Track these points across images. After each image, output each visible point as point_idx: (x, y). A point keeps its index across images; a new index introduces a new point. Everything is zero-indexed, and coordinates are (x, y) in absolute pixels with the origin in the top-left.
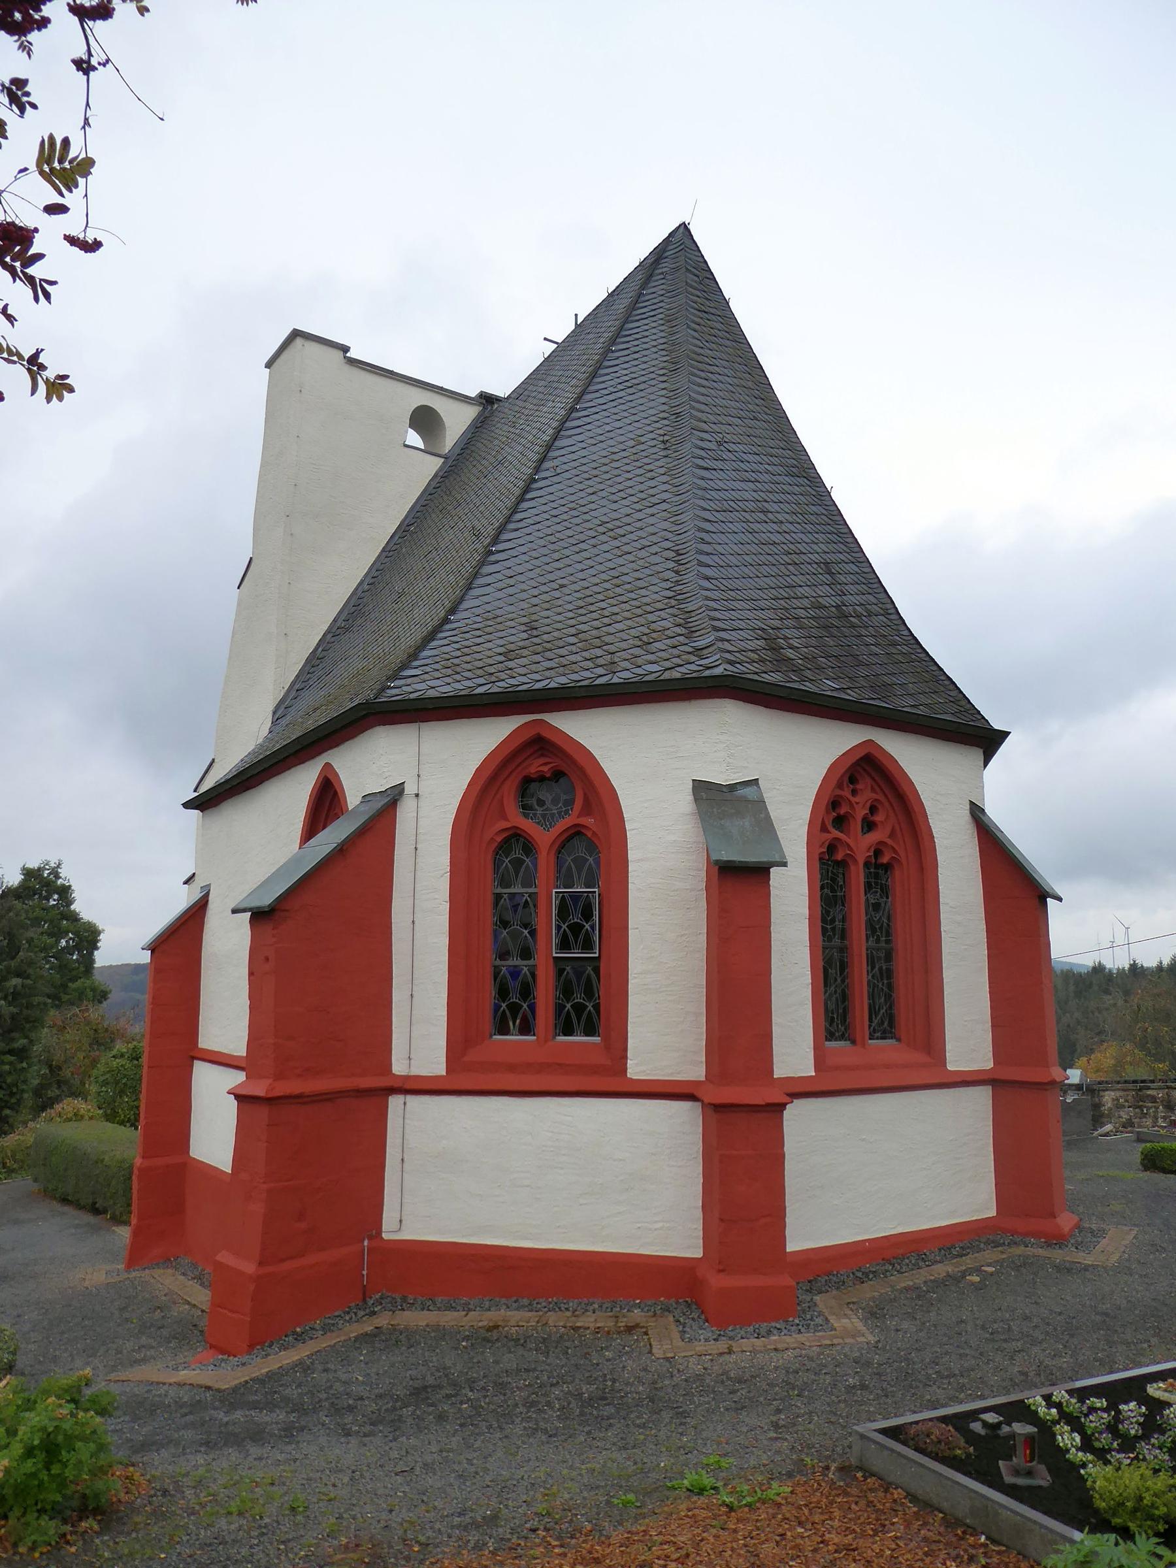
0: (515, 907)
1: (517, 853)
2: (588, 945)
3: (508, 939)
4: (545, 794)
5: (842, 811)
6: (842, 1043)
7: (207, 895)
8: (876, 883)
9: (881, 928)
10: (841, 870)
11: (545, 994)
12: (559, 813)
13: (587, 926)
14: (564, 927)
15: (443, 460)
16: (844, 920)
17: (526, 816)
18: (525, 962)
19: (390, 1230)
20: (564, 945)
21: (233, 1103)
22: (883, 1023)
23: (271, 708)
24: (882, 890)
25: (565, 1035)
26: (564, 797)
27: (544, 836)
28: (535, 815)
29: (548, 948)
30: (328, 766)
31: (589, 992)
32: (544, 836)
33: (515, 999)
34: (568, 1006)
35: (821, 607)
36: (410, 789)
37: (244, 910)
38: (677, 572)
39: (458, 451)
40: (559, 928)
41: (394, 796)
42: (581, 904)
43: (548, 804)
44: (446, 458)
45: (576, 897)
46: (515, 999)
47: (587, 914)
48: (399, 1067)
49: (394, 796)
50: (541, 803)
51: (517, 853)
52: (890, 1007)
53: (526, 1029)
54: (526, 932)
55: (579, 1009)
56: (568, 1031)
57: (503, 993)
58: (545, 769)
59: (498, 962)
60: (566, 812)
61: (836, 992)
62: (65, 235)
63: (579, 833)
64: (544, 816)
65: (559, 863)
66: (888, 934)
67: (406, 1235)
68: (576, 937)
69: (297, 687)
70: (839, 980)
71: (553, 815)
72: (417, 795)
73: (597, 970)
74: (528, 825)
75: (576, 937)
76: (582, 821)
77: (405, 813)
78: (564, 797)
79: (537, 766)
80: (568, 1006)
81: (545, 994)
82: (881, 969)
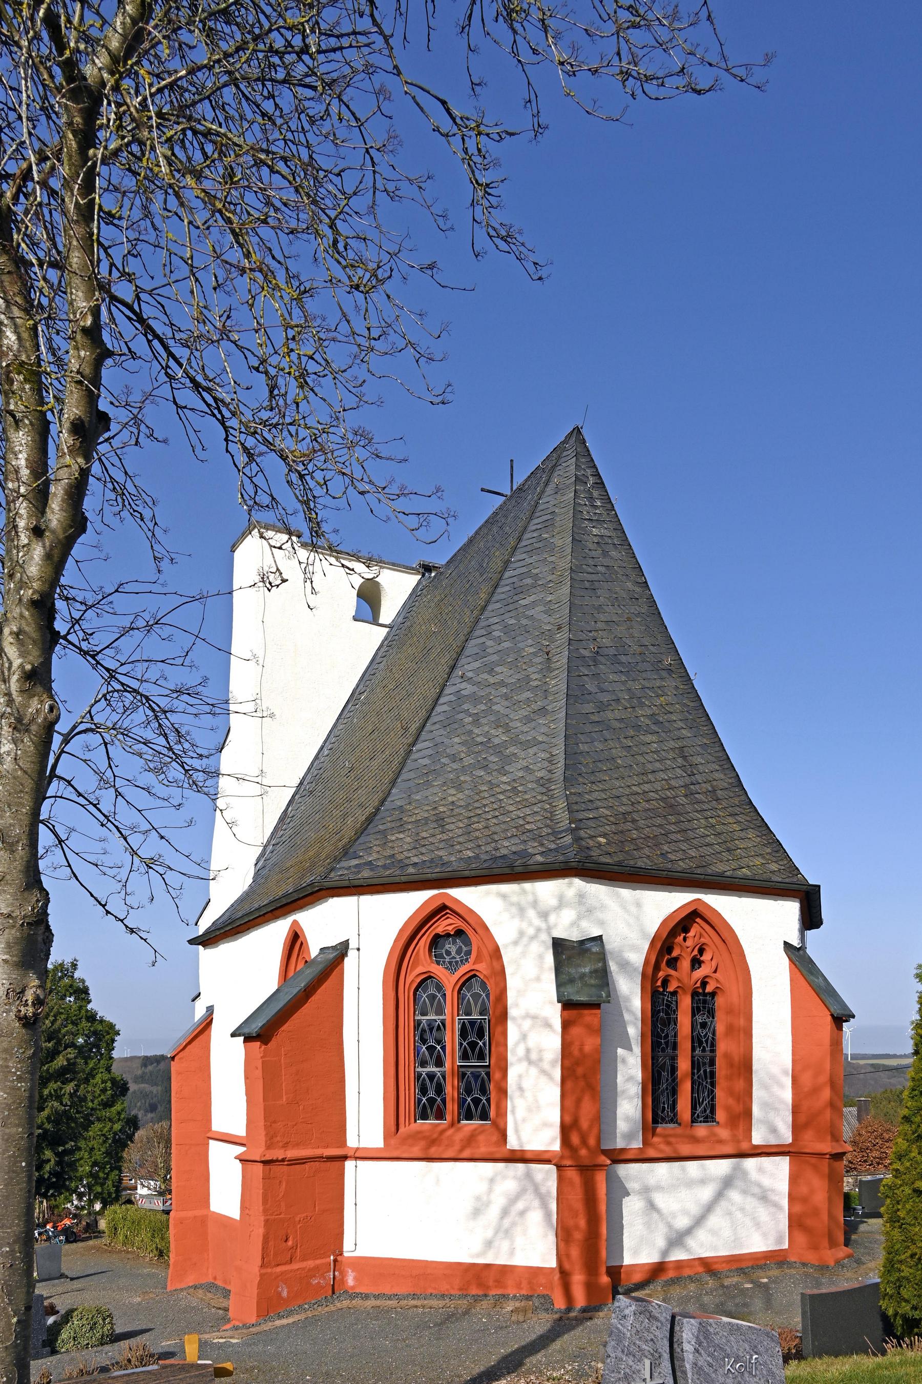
0: (431, 1030)
1: (432, 990)
2: (481, 1057)
3: (426, 1053)
4: (451, 947)
5: (675, 954)
6: (672, 1125)
7: (212, 1013)
8: (705, 1008)
9: (707, 1041)
10: (674, 998)
11: (451, 1089)
12: (462, 961)
13: (481, 1043)
14: (465, 1044)
15: (388, 629)
16: (676, 1035)
17: (438, 963)
18: (438, 1069)
19: (349, 1248)
20: (465, 1056)
21: (238, 1165)
22: (705, 1111)
23: (254, 862)
24: (708, 1012)
25: (467, 1120)
26: (465, 949)
27: (449, 980)
28: (444, 962)
29: (452, 1060)
30: (295, 923)
31: (484, 1090)
32: (449, 980)
33: (431, 1094)
34: (469, 1099)
35: (671, 788)
36: (353, 945)
37: (239, 1035)
38: (550, 771)
39: (400, 619)
40: (461, 1044)
41: (342, 950)
42: (477, 1026)
43: (453, 954)
44: (390, 626)
45: (472, 1023)
46: (431, 1094)
47: (481, 1035)
48: (352, 1142)
49: (342, 950)
50: (448, 953)
51: (432, 990)
52: (712, 1099)
53: (440, 1116)
54: (439, 1047)
55: (476, 1101)
56: (424, 1116)
57: (424, 1091)
58: (450, 928)
59: (419, 1069)
60: (467, 960)
61: (667, 1089)
62: (212, 1006)
63: (475, 976)
64: (450, 963)
65: (461, 997)
66: (713, 1045)
67: (359, 1253)
68: (473, 1051)
69: (273, 842)
70: (670, 1080)
71: (457, 962)
72: (358, 949)
73: (488, 1074)
74: (438, 971)
75: (473, 1051)
76: (476, 967)
77: (349, 963)
78: (465, 949)
79: (443, 926)
80: (424, 1099)
81: (451, 1089)
82: (705, 1071)
